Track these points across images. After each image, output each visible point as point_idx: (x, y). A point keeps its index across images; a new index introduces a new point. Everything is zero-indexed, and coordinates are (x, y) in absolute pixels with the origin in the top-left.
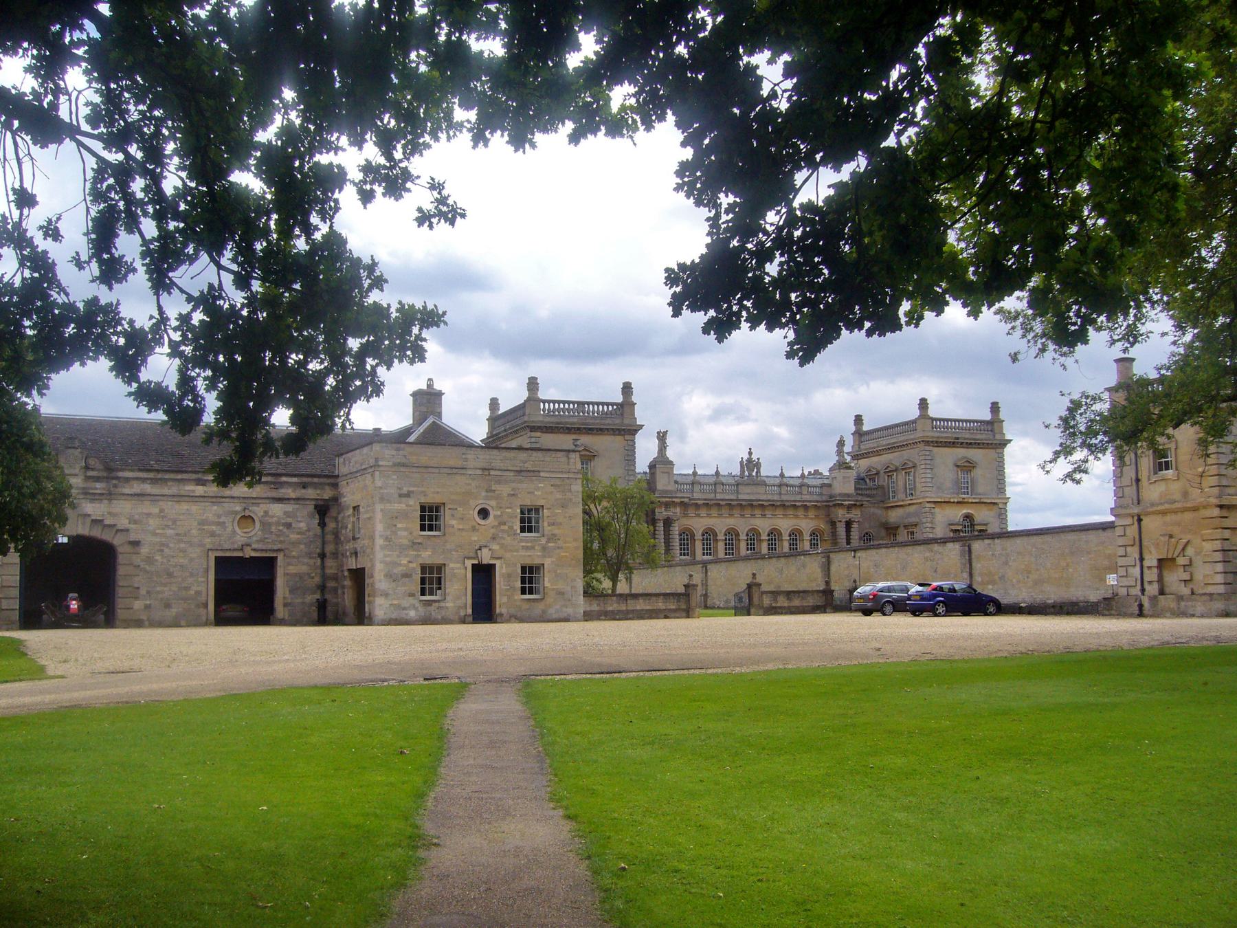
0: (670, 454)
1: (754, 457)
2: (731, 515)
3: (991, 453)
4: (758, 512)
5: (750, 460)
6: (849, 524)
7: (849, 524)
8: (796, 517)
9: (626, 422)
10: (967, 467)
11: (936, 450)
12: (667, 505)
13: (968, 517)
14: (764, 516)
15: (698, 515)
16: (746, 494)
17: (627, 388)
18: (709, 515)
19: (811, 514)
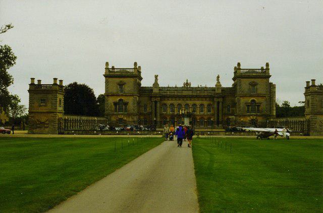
0: (159, 82)
1: (189, 82)
2: (179, 100)
3: (265, 80)
4: (189, 99)
5: (187, 83)
6: (218, 103)
7: (218, 103)
8: (202, 100)
9: (267, 74)
10: (253, 85)
11: (242, 79)
12: (156, 97)
13: (253, 101)
14: (191, 100)
15: (168, 100)
16: (185, 93)
17: (267, 65)
18: (172, 100)
19: (208, 99)
